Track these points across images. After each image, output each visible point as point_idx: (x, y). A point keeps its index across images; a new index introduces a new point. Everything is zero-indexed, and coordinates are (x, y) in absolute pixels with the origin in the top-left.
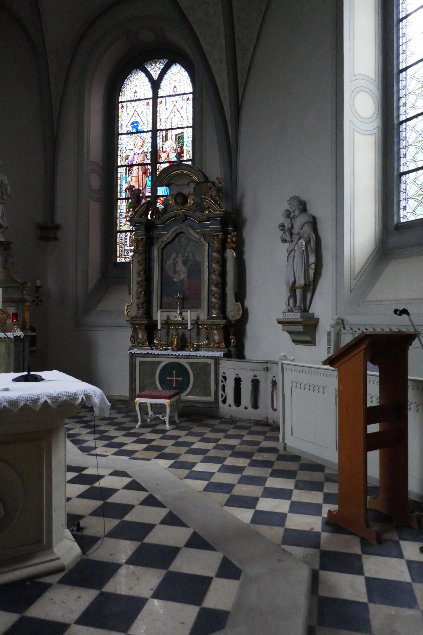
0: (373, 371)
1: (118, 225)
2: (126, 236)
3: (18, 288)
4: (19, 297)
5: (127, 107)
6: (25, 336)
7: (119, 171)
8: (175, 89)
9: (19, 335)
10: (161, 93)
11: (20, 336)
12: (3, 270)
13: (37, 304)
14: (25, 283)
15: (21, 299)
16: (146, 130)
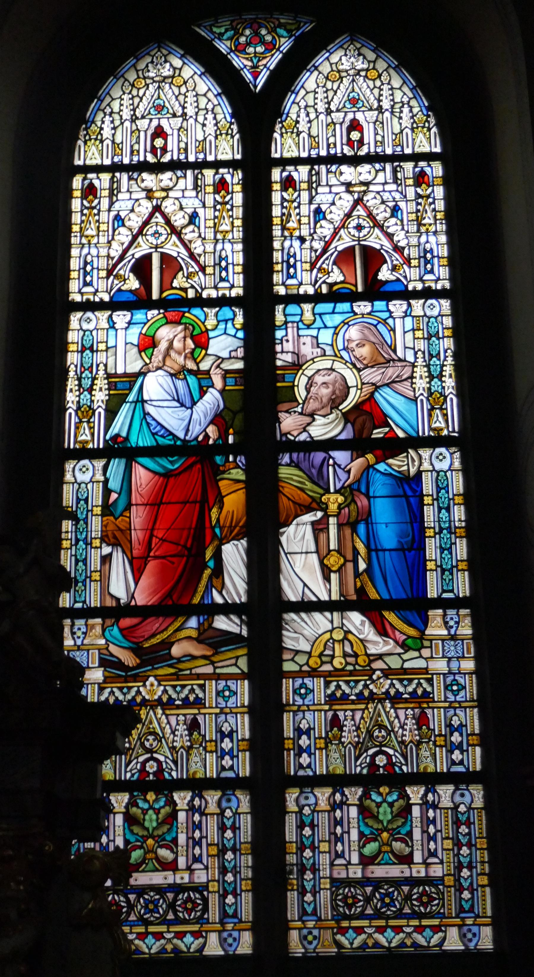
1: (288, 744)
2: (341, 805)
5: (113, 193)
7: (68, 477)
10: (284, 146)
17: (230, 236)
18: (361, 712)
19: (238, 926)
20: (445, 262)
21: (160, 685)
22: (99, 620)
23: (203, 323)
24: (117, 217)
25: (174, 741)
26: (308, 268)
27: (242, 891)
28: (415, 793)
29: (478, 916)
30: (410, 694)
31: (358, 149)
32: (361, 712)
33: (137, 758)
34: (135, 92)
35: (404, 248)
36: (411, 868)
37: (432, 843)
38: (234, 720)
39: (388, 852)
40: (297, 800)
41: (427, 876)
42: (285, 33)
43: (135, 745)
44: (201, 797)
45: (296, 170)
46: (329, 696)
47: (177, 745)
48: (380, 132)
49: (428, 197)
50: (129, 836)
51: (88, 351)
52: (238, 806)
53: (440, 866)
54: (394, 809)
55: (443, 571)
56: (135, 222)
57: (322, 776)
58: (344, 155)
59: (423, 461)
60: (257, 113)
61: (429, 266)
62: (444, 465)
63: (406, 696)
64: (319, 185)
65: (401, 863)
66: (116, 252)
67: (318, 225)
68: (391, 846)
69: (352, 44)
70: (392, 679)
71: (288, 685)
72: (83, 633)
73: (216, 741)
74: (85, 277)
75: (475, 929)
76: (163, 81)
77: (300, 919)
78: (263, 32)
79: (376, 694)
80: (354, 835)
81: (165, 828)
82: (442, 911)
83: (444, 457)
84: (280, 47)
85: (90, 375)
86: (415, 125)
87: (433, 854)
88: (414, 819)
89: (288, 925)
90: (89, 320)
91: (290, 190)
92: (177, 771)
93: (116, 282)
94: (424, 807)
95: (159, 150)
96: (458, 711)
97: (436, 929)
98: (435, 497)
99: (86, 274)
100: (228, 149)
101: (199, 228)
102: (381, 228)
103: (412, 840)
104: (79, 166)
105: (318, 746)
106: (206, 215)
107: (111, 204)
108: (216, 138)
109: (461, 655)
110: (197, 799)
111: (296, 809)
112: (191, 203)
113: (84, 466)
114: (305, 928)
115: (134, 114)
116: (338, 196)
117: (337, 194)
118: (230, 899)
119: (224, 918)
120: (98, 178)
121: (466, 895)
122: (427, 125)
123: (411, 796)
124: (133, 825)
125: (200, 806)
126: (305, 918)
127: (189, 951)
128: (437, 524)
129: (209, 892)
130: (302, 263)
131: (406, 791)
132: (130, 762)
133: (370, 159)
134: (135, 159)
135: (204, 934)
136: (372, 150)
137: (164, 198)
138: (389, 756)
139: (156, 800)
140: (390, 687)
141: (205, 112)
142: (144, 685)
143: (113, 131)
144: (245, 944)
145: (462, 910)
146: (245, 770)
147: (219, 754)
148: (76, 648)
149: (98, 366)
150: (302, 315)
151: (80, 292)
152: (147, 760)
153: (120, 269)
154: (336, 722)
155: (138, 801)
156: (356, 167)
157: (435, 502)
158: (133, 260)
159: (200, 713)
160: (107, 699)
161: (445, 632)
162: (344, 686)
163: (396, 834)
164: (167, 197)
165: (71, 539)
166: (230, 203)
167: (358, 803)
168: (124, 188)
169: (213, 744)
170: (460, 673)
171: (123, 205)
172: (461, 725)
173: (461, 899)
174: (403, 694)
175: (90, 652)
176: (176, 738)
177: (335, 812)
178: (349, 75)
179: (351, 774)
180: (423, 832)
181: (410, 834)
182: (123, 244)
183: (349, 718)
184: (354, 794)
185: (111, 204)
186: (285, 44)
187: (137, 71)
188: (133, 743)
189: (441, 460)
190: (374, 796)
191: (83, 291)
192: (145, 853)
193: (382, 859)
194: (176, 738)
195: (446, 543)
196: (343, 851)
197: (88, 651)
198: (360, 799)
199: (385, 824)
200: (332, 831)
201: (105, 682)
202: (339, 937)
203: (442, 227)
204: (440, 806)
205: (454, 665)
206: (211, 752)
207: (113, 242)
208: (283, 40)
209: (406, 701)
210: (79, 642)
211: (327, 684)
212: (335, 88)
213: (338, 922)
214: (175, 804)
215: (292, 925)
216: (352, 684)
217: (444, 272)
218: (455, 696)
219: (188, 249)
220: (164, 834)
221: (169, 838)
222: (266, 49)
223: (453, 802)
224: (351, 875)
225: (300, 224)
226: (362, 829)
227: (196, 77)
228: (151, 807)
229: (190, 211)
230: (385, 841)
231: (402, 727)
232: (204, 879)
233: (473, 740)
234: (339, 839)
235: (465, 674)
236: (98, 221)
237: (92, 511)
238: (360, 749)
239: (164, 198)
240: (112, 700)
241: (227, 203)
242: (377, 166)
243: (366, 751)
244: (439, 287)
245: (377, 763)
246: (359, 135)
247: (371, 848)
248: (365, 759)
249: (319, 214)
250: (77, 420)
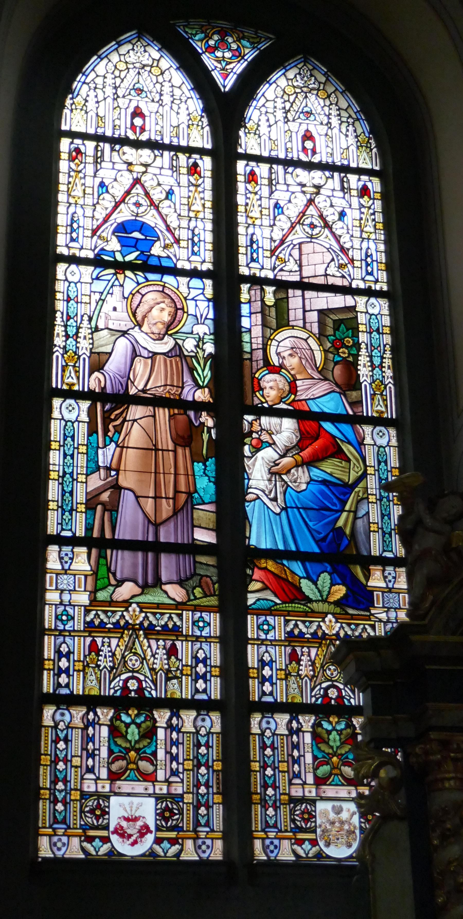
1: (253, 673)
2: (93, 724)
5: (98, 160)
7: (56, 414)
17: (201, 215)
18: (117, 640)
19: (211, 835)
20: (383, 267)
21: (337, 622)
22: (84, 549)
23: (177, 289)
24: (102, 185)
25: (154, 663)
26: (90, 235)
27: (214, 803)
28: (162, 717)
30: (113, 624)
31: (141, 133)
32: (117, 640)
33: (320, 684)
34: (117, 73)
35: (348, 249)
36: (154, 786)
37: (296, 766)
38: (208, 647)
39: (337, 775)
40: (260, 723)
41: (169, 793)
42: (248, 44)
43: (119, 664)
44: (178, 717)
45: (201, 159)
46: (288, 633)
47: (157, 667)
48: (160, 122)
49: (256, 193)
50: (316, 753)
51: (375, 333)
52: (212, 726)
53: (181, 785)
54: (141, 730)
55: (384, 533)
56: (118, 191)
57: (282, 703)
58: (127, 138)
59: (81, 412)
60: (226, 112)
61: (369, 269)
62: (383, 442)
63: (109, 626)
64: (278, 183)
65: (145, 780)
66: (100, 214)
67: (101, 197)
68: (137, 764)
69: (305, 65)
70: (146, 613)
71: (251, 621)
72: (70, 558)
73: (54, 660)
74: (193, 247)
76: (143, 68)
77: (263, 830)
78: (230, 40)
79: (327, 634)
80: (104, 753)
81: (145, 742)
82: (181, 825)
83: (73, 409)
84: (244, 55)
85: (75, 324)
86: (190, 122)
87: (174, 773)
88: (159, 742)
89: (252, 834)
90: (373, 306)
91: (366, 197)
92: (355, 699)
93: (99, 242)
94: (169, 731)
95: (138, 129)
96: (269, 649)
97: (173, 842)
98: (62, 444)
99: (73, 230)
100: (201, 137)
101: (175, 204)
102: (330, 228)
103: (157, 760)
104: (241, 154)
105: (77, 668)
106: (181, 193)
107: (271, 193)
108: (188, 127)
109: (72, 588)
110: (174, 719)
111: (259, 732)
112: (340, 203)
113: (70, 405)
114: (268, 838)
115: (116, 93)
116: (120, 173)
117: (119, 171)
118: (203, 811)
119: (197, 827)
120: (83, 144)
121: (60, 807)
122: (200, 123)
123: (158, 719)
124: (117, 737)
125: (177, 725)
126: (55, 826)
127: (165, 856)
128: (61, 468)
129: (184, 803)
130: (378, 263)
131: (153, 715)
132: (315, 687)
133: (322, 167)
134: (117, 133)
135: (180, 841)
136: (123, 134)
137: (144, 173)
138: (139, 681)
139: (137, 716)
140: (144, 620)
141: (346, 124)
142: (324, 621)
143: (97, 105)
144: (216, 852)
145: (267, 825)
146: (216, 693)
147: (194, 677)
148: (63, 572)
149: (82, 316)
150: (204, 289)
151: (247, 265)
152: (328, 687)
153: (103, 232)
154: (94, 648)
155: (323, 722)
156: (309, 172)
157: (62, 448)
158: (115, 224)
159: (177, 640)
160: (360, 635)
161: (384, 585)
162: (151, 618)
163: (143, 753)
164: (146, 172)
165: (59, 471)
166: (83, 171)
167: (109, 723)
168: (107, 157)
169: (51, 662)
170: (70, 605)
171: (106, 173)
172: (272, 661)
173: (55, 810)
174: (106, 624)
175: (77, 577)
176: (155, 661)
177: (87, 729)
178: (302, 91)
179: (105, 696)
180: (167, 752)
181: (155, 754)
182: (106, 209)
183: (106, 645)
184: (105, 714)
185: (271, 193)
186: (250, 55)
187: (120, 55)
188: (117, 662)
189: (70, 411)
190: (124, 717)
191: (250, 265)
192: (332, 769)
193: (333, 780)
194: (155, 661)
195: (386, 510)
196: (300, 772)
197: (75, 575)
198: (111, 720)
199: (133, 744)
200: (84, 747)
201: (91, 605)
202: (295, 847)
203: (209, 215)
204: (183, 730)
205: (66, 597)
206: (187, 675)
207: (97, 206)
208: (247, 51)
209: (158, 633)
210: (390, 585)
211: (287, 622)
212: (122, 77)
213: (84, 830)
214: (155, 721)
215: (42, 831)
216: (158, 616)
217: (383, 276)
218: (266, 634)
219: (165, 221)
220: (346, 753)
221: (149, 751)
222: (233, 56)
223: (260, 728)
224: (100, 789)
225: (262, 215)
226: (315, 753)
227: (172, 70)
228: (334, 729)
229: (167, 188)
230: (133, 759)
231: (153, 656)
232: (180, 791)
233: (49, 665)
234: (296, 761)
235: (74, 606)
236: (84, 184)
237: (60, 446)
238: (315, 682)
239: (144, 173)
240: (365, 635)
241: (80, 172)
242: (327, 173)
243: (120, 675)
244: (378, 287)
245: (330, 695)
246: (134, 121)
247: (324, 769)
248: (118, 683)
249: (102, 188)
250: (64, 364)
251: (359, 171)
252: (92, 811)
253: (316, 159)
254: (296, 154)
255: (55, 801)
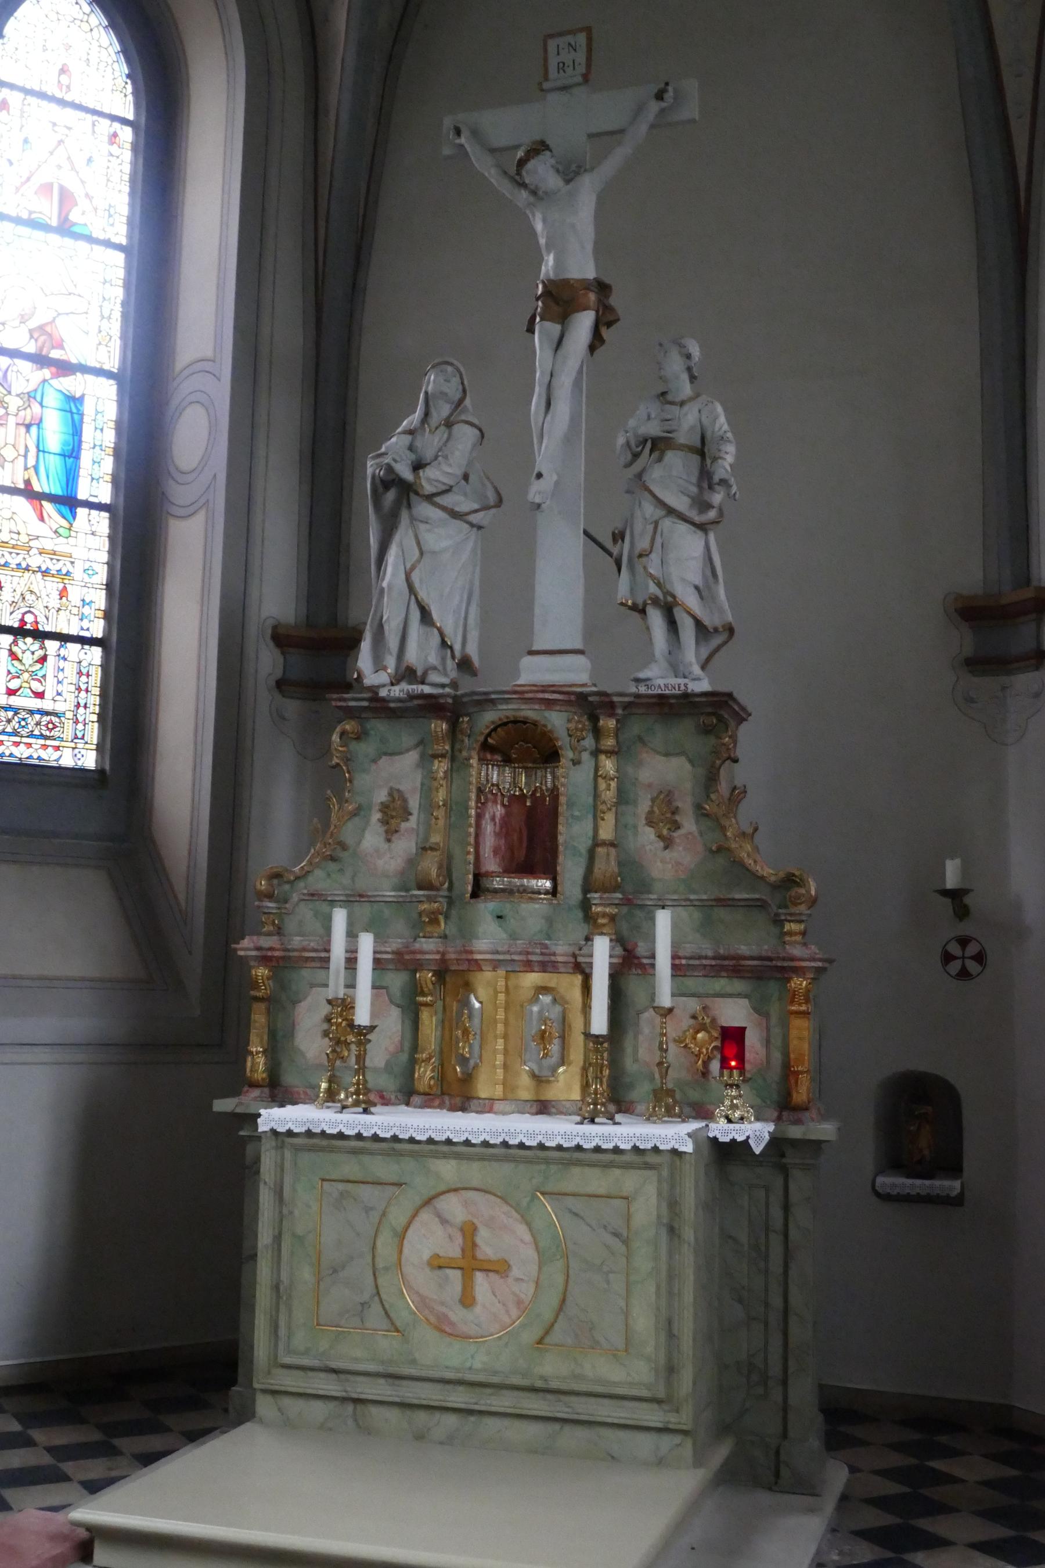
0: (211, 1523)
3: (761, 905)
4: (766, 949)
6: (776, 1143)
8: (64, 79)
9: (740, 1138)
11: (746, 1142)
12: (697, 822)
13: (964, 974)
14: (790, 881)
15: (770, 959)
16: (102, 236)
29: (86, 743)
47: (50, 606)
75: (83, 752)
145: (76, 738)
248: (17, 616)
251: (114, 118)
252: (55, 727)
253: (68, 98)
254: (51, 89)
255: (77, 722)
